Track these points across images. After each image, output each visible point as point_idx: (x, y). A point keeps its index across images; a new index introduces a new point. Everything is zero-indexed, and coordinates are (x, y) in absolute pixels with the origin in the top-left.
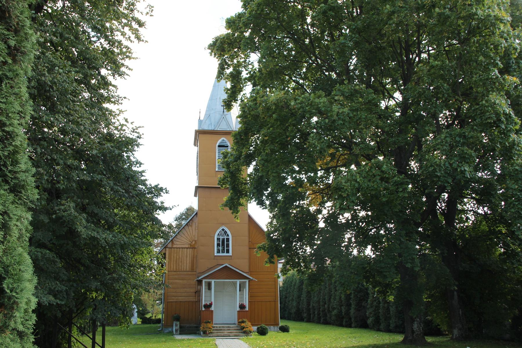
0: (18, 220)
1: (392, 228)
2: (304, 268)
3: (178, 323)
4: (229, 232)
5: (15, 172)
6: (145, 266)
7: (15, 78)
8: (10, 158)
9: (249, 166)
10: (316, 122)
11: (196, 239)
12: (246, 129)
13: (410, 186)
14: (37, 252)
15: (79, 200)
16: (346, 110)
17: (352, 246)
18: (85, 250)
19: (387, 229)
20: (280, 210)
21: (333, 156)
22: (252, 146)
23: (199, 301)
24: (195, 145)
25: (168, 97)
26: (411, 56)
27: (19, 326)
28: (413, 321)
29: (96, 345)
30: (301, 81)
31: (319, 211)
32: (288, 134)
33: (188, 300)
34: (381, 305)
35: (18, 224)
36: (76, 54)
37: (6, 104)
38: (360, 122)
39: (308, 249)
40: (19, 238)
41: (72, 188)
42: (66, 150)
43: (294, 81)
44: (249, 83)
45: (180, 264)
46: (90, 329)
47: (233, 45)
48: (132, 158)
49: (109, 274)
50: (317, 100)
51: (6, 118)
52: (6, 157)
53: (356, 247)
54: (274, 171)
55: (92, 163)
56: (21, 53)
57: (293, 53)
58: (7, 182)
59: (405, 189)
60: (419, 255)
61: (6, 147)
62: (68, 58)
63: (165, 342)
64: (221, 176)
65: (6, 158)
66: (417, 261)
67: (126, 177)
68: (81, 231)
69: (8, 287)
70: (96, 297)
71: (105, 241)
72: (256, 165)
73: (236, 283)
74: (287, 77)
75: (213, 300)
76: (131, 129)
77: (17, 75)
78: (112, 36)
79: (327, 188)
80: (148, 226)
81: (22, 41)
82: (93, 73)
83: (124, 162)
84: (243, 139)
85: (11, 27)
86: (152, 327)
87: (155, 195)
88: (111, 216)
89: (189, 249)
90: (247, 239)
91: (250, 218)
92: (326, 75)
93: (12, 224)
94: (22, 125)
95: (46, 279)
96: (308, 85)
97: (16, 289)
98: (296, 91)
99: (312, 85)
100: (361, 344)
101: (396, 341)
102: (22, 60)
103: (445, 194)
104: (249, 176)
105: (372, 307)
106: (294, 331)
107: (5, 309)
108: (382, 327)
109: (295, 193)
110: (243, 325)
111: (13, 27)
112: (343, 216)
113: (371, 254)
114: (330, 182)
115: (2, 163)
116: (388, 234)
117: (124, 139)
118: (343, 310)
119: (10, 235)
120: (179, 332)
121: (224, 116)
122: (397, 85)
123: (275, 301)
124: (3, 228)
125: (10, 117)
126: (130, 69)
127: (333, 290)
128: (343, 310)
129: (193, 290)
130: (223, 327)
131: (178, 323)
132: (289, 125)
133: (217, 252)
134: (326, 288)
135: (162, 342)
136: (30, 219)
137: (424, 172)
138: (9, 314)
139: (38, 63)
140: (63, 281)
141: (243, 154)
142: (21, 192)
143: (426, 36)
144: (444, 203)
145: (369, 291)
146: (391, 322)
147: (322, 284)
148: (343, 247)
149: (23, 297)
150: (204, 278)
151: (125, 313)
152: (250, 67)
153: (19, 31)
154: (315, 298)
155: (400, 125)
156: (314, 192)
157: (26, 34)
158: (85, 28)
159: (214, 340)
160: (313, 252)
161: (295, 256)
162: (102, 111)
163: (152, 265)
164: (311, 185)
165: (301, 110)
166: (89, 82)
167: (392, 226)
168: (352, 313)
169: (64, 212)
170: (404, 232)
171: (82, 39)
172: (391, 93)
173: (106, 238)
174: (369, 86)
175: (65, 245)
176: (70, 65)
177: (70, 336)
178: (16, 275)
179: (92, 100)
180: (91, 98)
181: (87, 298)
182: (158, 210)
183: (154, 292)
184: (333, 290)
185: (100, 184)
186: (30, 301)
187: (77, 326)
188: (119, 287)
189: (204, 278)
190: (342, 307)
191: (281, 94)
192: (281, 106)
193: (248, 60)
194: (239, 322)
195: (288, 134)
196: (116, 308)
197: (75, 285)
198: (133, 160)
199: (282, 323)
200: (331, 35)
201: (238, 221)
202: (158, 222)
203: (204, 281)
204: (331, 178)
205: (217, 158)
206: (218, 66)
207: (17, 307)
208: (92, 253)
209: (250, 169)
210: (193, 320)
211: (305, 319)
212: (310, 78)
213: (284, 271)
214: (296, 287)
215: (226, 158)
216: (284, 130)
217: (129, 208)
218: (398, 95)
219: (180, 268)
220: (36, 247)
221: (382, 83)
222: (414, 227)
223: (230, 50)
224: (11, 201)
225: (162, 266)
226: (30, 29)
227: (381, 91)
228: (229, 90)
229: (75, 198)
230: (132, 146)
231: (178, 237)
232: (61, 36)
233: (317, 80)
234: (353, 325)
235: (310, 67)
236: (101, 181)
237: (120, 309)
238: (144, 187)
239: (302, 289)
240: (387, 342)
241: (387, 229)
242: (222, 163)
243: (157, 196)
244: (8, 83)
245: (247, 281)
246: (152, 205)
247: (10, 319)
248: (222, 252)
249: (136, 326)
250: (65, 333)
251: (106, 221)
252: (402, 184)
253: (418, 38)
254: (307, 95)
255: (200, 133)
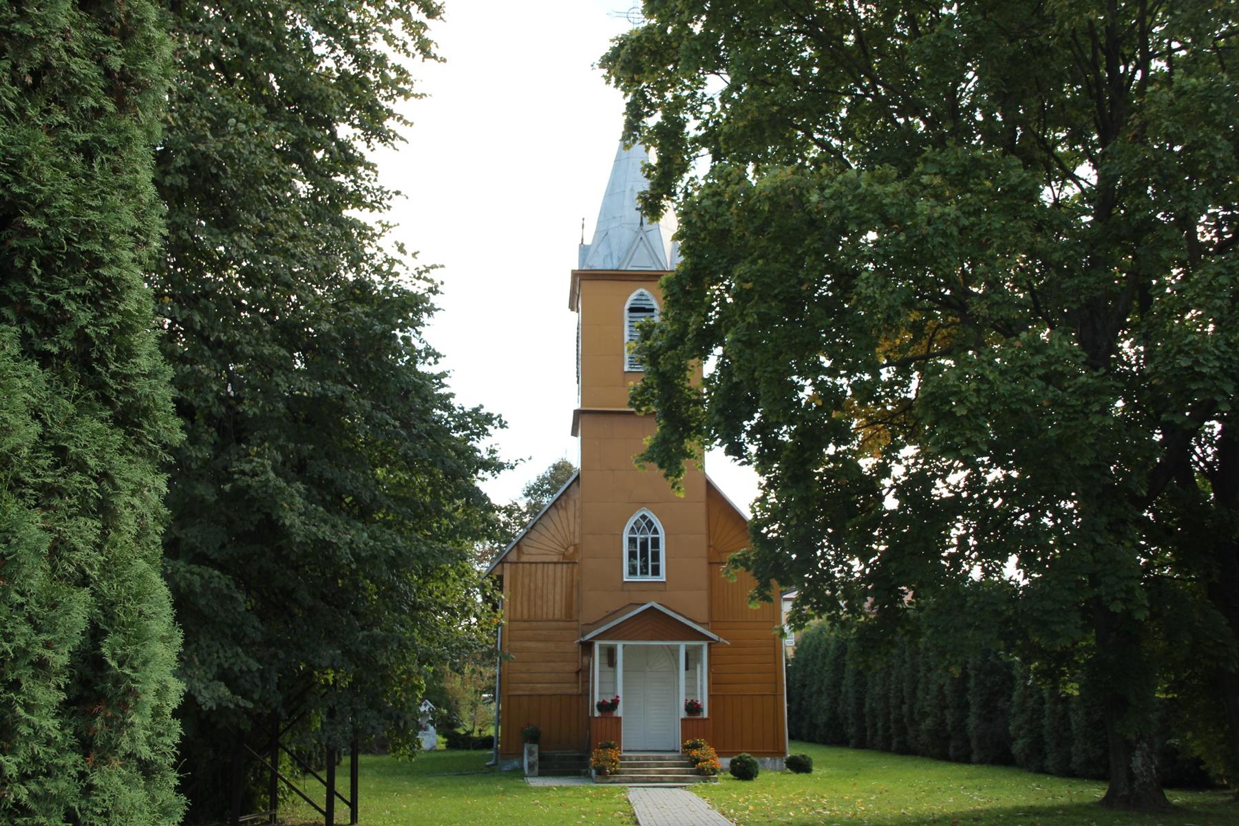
0: (133, 493)
1: (1071, 510)
2: (846, 613)
3: (535, 748)
4: (658, 524)
5: (127, 377)
6: (453, 608)
7: (123, 147)
8: (113, 343)
9: (707, 359)
10: (873, 242)
11: (577, 541)
12: (695, 267)
13: (1120, 404)
14: (192, 573)
15: (291, 446)
16: (951, 210)
17: (969, 557)
18: (307, 568)
19: (1058, 513)
20: (789, 468)
21: (917, 328)
22: (713, 308)
23: (586, 694)
24: (572, 307)
25: (503, 189)
26: (1122, 68)
27: (140, 748)
28: (1130, 748)
29: (337, 799)
30: (835, 143)
31: (883, 470)
32: (802, 274)
33: (559, 692)
34: (1047, 706)
35: (136, 501)
36: (277, 88)
37: (101, 212)
38: (988, 240)
39: (857, 565)
40: (138, 537)
41: (276, 415)
42: (256, 324)
43: (817, 142)
44: (705, 151)
45: (539, 602)
46: (318, 762)
47: (661, 55)
48: (415, 342)
49: (363, 629)
50: (878, 189)
51: (103, 245)
52: (103, 340)
53: (977, 560)
54: (769, 369)
55: (319, 354)
56: (137, 86)
57: (815, 70)
58: (106, 401)
59: (1105, 411)
60: (1145, 581)
61: (103, 315)
62: (257, 99)
63: (503, 793)
64: (635, 383)
65: (103, 344)
66: (1142, 597)
67: (402, 389)
68: (292, 526)
69: (114, 655)
70: (335, 681)
71: (351, 548)
72: (724, 356)
73: (677, 648)
74: (799, 133)
75: (620, 693)
76: (413, 271)
77: (128, 140)
78: (362, 42)
79: (903, 412)
80: (457, 509)
81: (139, 57)
82: (318, 135)
83: (397, 352)
84: (689, 293)
85: (112, 24)
86: (477, 759)
87: (473, 433)
88: (365, 486)
89: (559, 566)
90: (702, 539)
91: (711, 489)
92: (899, 124)
93: (122, 504)
94: (141, 263)
95: (212, 639)
96: (854, 151)
97: (132, 658)
98: (824, 165)
99: (862, 151)
100: (994, 804)
101: (1087, 801)
102: (139, 105)
103: (1213, 422)
104: (707, 382)
105: (1022, 712)
106: (824, 771)
107: (108, 706)
108: (1049, 763)
109: (823, 424)
110: (695, 753)
111: (118, 25)
112: (944, 482)
113: (1020, 578)
114: (912, 396)
115: (94, 356)
116: (1062, 525)
117: (395, 295)
118: (949, 720)
119: (117, 530)
120: (537, 769)
121: (642, 235)
122: (1084, 146)
123: (776, 696)
124: (99, 512)
125: (111, 242)
126: (406, 123)
127: (922, 669)
128: (949, 720)
129: (572, 667)
130: (646, 758)
131: (535, 748)
132: (805, 253)
133: (630, 574)
134: (904, 662)
135: (497, 792)
136: (165, 490)
137: (1161, 369)
138: (118, 718)
139: (188, 110)
140: (253, 643)
141: (690, 329)
142: (140, 426)
143: (1165, 14)
144: (1212, 446)
145: (1014, 672)
146: (1073, 749)
147: (895, 651)
148: (945, 559)
149: (148, 678)
150: (598, 637)
151: (402, 724)
152: (706, 108)
153: (132, 33)
154: (877, 688)
155: (1093, 246)
156: (871, 422)
157: (148, 40)
158: (298, 23)
159: (623, 790)
160: (868, 571)
161: (824, 581)
162: (341, 227)
163: (470, 605)
164: (862, 404)
165: (837, 214)
166: (310, 157)
167: (1070, 505)
168: (971, 727)
169: (253, 477)
170: (1104, 520)
171: (290, 52)
172: (1069, 165)
173: (352, 541)
174: (1010, 148)
175: (256, 557)
176: (264, 115)
177: (275, 776)
178: (132, 624)
179: (316, 202)
180: (314, 196)
181: (315, 683)
182: (481, 471)
183: (473, 671)
184: (922, 669)
185: (339, 407)
186: (166, 688)
187: (290, 753)
188: (388, 659)
189: (598, 637)
190: (946, 712)
191: (785, 173)
192: (784, 201)
193: (700, 92)
194: (685, 747)
195: (802, 274)
196: (380, 711)
197: (281, 654)
198: (419, 346)
199: (792, 750)
200: (911, 21)
201: (682, 495)
202: (478, 499)
203: (597, 644)
204: (914, 385)
205: (627, 338)
206: (624, 109)
207: (137, 703)
208: (324, 574)
209: (710, 366)
210: (568, 741)
211: (853, 741)
212: (857, 133)
213: (798, 620)
214: (827, 661)
215: (648, 339)
216: (793, 266)
217: (408, 463)
218: (1086, 172)
219: (539, 612)
220: (190, 563)
221: (1044, 141)
222: (1130, 507)
223: (656, 69)
224: (116, 447)
225: (495, 607)
226: (158, 27)
227: (1043, 161)
228: (654, 169)
229: (281, 442)
230: (415, 314)
231: (534, 535)
232: (243, 42)
233: (875, 139)
234: (975, 757)
235: (857, 104)
236: (342, 398)
237: (389, 717)
238: (446, 414)
239: (844, 665)
240: (1063, 800)
241: (1058, 513)
242: (638, 352)
243: (478, 435)
244: (108, 160)
245: (705, 644)
246: (466, 458)
247: (119, 731)
248: (642, 573)
249: (434, 755)
250: (262, 769)
251: (357, 500)
252: (1098, 392)
253: (1141, 20)
254: (851, 174)
255: (584, 279)
